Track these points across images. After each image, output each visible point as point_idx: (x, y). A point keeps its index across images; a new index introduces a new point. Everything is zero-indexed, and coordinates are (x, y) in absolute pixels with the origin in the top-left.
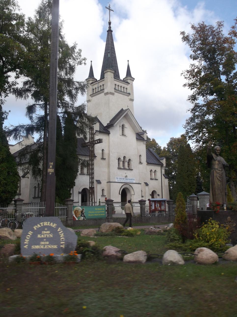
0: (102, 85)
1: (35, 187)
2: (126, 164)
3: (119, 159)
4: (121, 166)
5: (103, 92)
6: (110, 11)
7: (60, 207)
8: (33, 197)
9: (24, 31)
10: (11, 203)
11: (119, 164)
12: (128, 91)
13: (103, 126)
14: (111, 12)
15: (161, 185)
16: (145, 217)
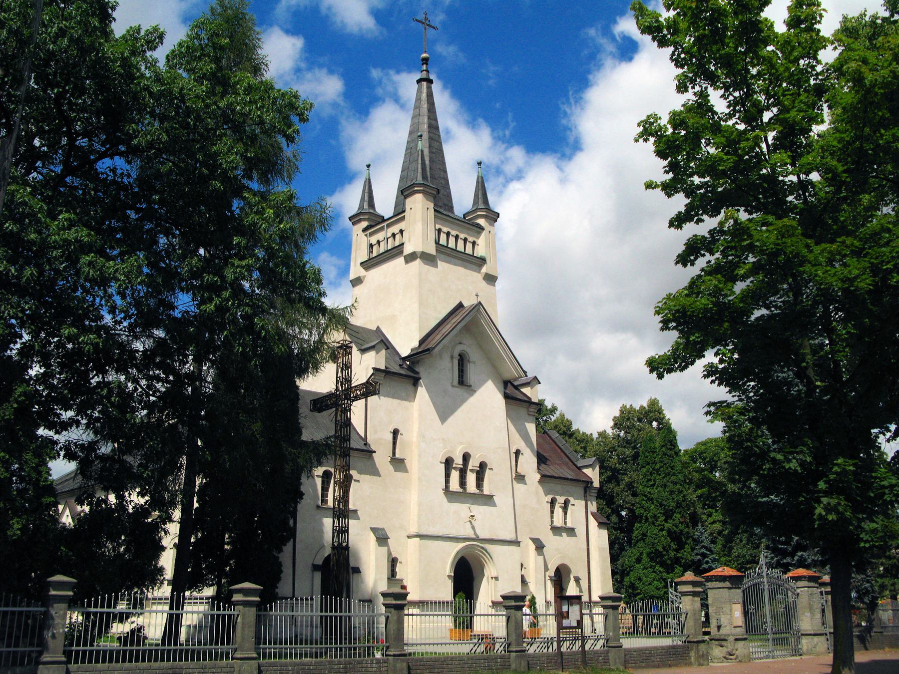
2: (471, 478)
3: (448, 463)
4: (455, 485)
7: (102, 607)
11: (447, 476)
12: (480, 251)
15: (586, 547)
16: (524, 651)
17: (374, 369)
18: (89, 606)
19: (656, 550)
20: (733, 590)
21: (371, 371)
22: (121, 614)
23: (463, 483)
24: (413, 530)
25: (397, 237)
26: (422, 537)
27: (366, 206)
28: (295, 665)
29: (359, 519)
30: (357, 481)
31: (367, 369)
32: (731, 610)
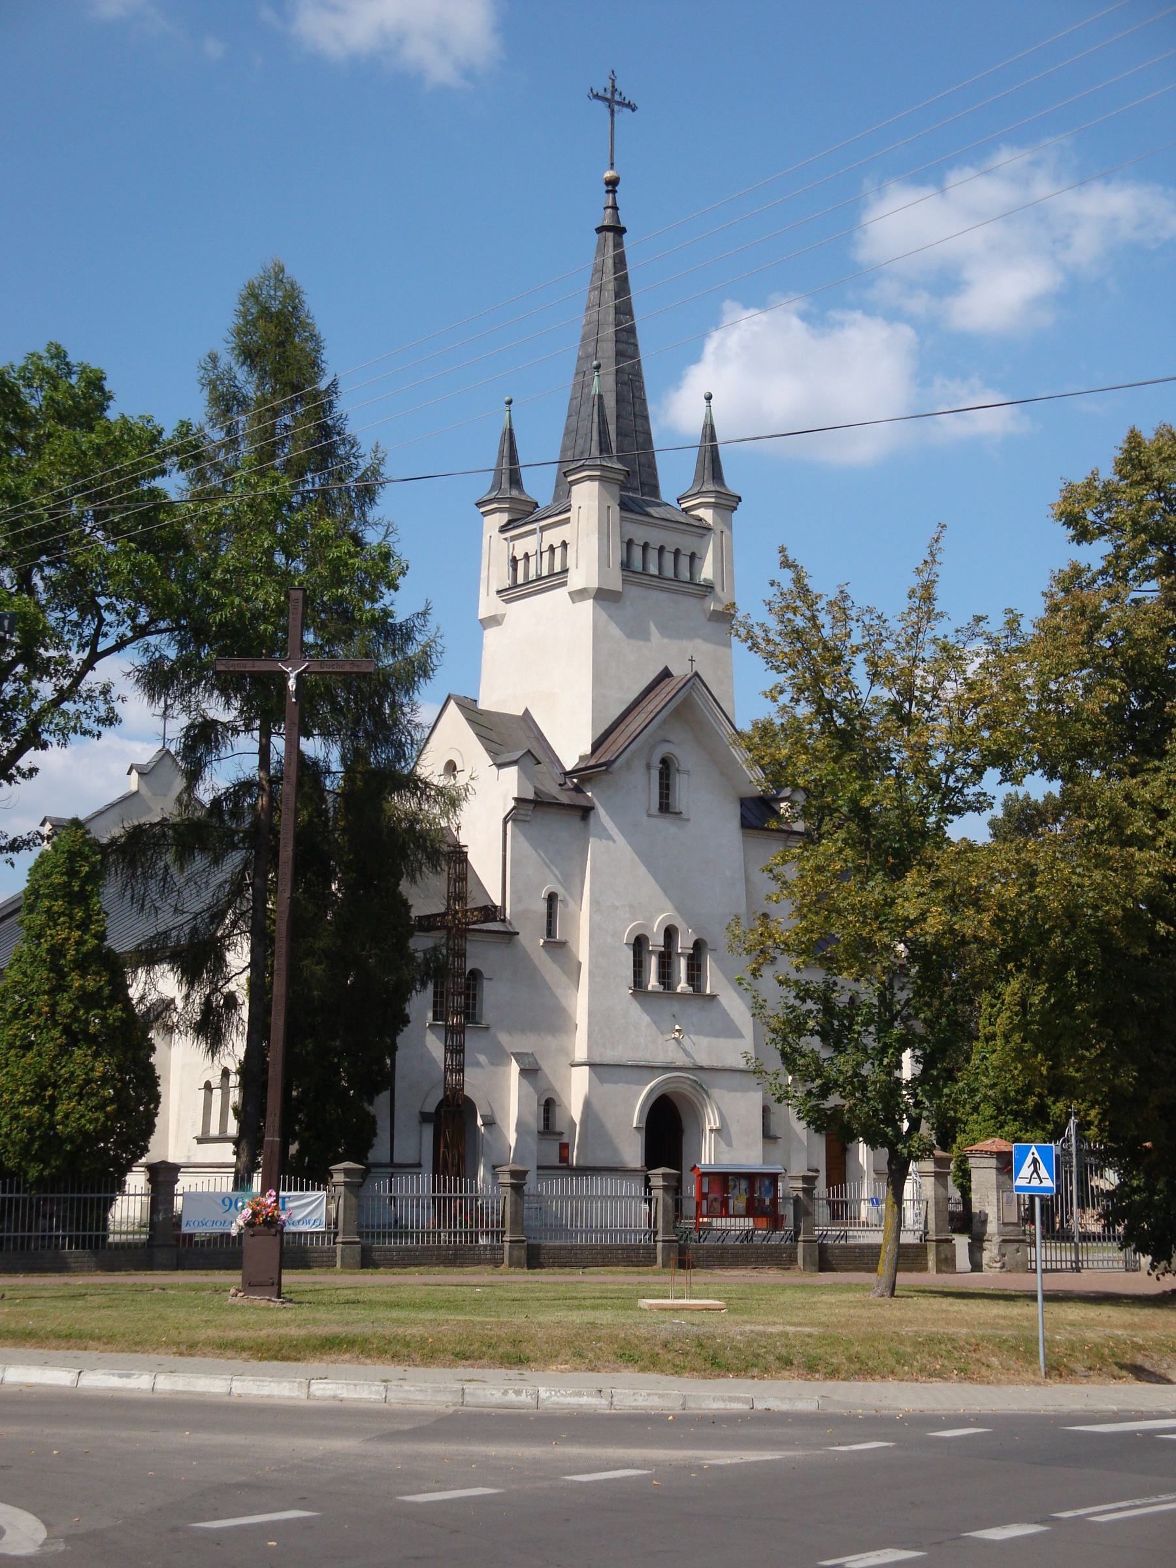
1: (208, 1087)
3: (639, 944)
4: (653, 982)
5: (564, 584)
6: (612, 112)
8: (199, 1133)
13: (563, 768)
14: (623, 114)
17: (516, 799)
21: (512, 804)
23: (666, 976)
25: (558, 552)
28: (399, 1250)
31: (505, 797)
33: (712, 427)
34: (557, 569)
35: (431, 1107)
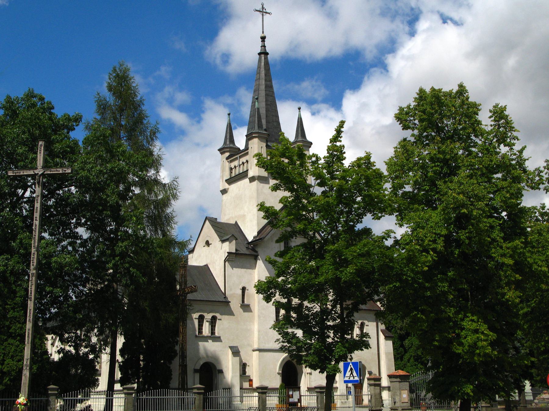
0: (245, 161)
6: (263, 15)
9: (475, 171)
10: (121, 334)
15: (377, 352)
18: (64, 396)
19: (417, 354)
20: (402, 383)
21: (227, 254)
22: (79, 400)
24: (256, 346)
26: (260, 350)
27: (228, 143)
29: (221, 341)
30: (220, 320)
31: (225, 252)
32: (400, 394)
33: (301, 119)
34: (245, 170)
35: (198, 367)
